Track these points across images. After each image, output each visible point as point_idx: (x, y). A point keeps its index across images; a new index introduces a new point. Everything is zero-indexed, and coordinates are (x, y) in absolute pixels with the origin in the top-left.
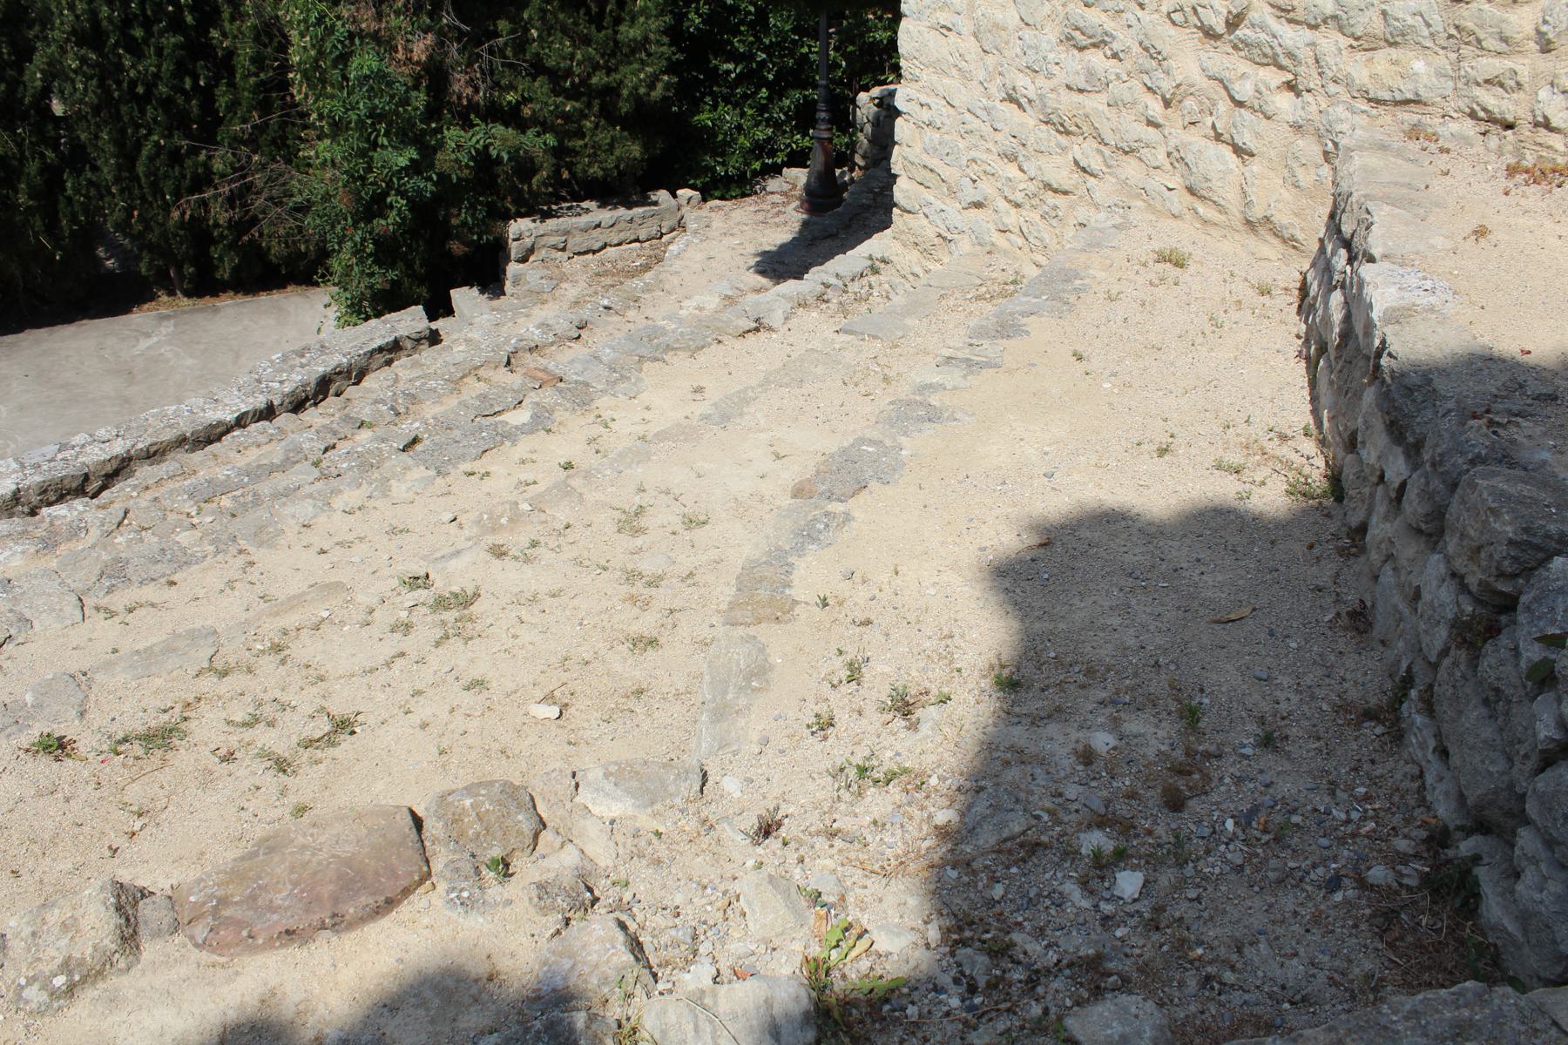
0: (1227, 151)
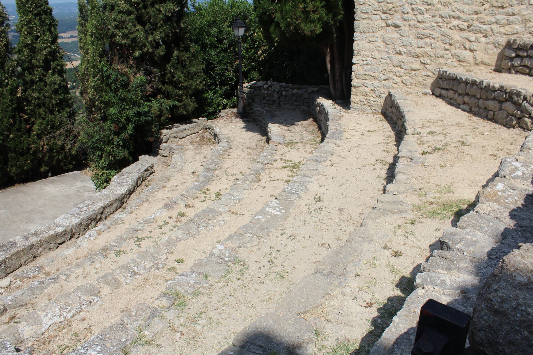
0: (468, 52)
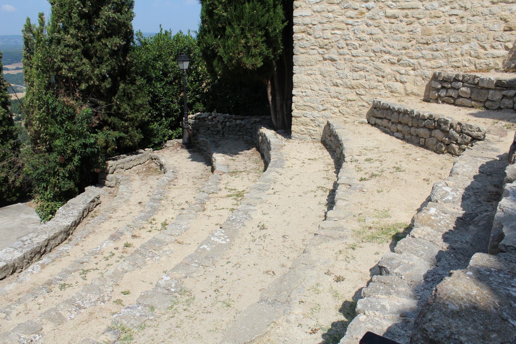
0: (399, 83)
